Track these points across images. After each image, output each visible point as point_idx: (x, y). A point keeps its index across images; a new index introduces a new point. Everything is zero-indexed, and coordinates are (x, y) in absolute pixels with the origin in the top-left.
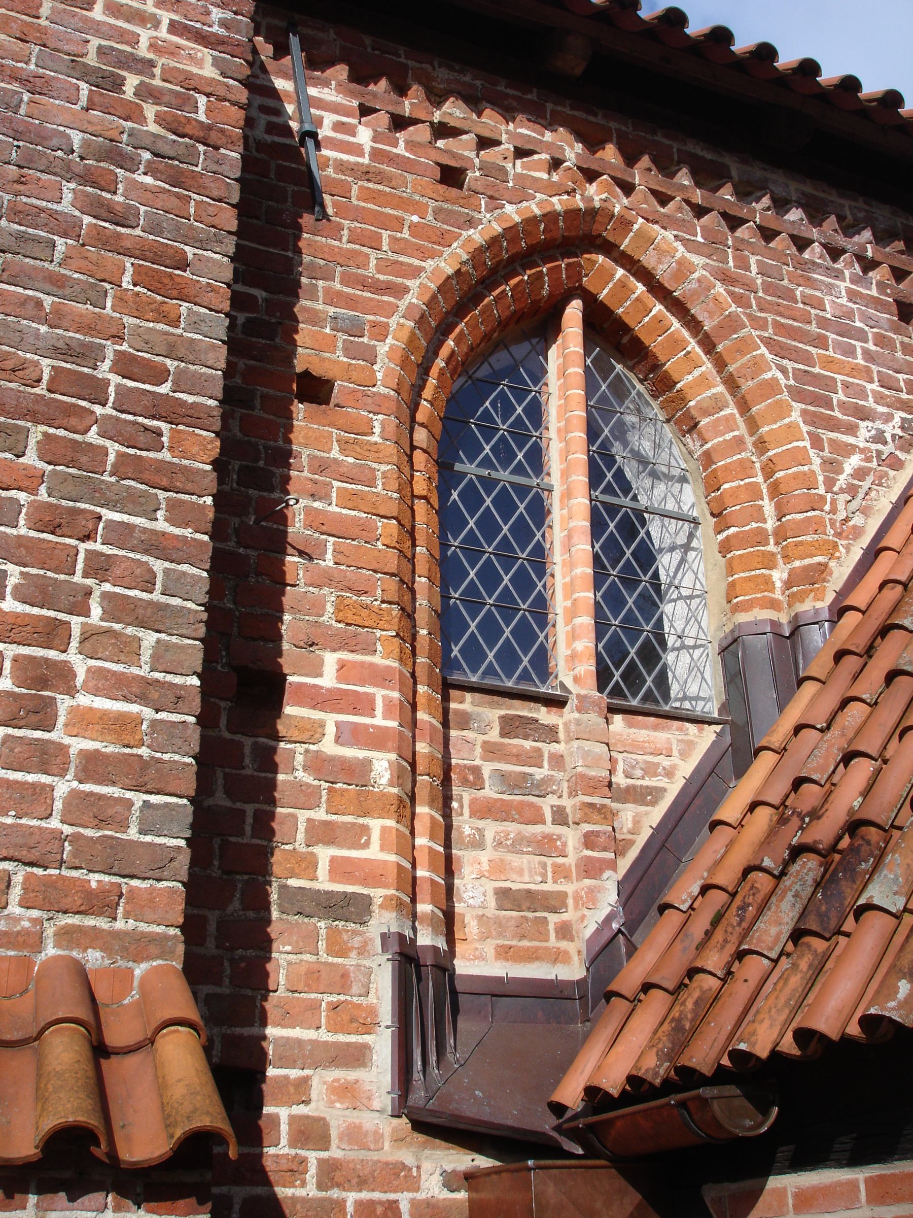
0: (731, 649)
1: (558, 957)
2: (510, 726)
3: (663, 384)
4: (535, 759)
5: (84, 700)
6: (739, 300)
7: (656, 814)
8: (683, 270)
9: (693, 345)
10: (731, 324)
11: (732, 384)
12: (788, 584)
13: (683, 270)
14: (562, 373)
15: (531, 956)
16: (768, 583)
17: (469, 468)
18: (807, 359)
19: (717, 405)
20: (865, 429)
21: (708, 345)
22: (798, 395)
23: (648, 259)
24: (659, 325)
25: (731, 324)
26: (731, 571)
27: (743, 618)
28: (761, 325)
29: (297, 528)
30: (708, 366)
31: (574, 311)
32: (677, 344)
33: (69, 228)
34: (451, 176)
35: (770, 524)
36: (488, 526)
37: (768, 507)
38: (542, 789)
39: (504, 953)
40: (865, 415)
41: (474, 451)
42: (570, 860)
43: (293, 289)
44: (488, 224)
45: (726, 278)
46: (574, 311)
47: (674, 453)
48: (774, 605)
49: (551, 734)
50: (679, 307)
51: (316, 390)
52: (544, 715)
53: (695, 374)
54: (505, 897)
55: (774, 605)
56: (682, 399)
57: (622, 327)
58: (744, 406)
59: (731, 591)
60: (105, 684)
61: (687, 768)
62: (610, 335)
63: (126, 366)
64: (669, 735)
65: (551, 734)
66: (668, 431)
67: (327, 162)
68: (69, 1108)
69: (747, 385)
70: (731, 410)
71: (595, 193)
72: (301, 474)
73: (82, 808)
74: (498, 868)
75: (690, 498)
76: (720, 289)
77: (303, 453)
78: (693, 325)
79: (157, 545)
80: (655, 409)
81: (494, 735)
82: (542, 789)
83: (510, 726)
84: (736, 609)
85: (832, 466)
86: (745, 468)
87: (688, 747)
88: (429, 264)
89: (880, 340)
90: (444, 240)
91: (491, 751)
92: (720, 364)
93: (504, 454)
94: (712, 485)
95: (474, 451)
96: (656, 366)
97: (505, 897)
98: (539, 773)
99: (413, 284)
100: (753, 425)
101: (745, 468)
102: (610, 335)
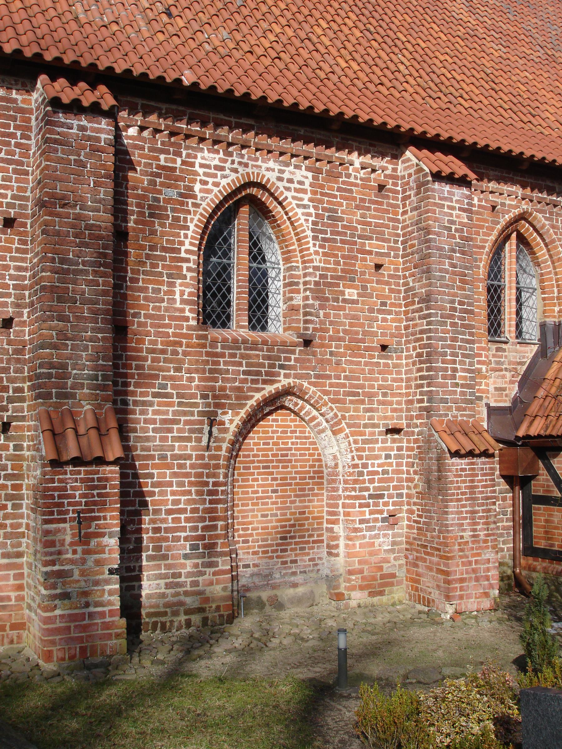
0: (543, 326)
1: (505, 401)
2: (498, 349)
3: (533, 253)
4: (501, 357)
5: (460, 374)
6: (556, 233)
7: (525, 368)
8: (544, 226)
9: (542, 245)
10: (553, 241)
11: (551, 256)
12: (559, 312)
13: (544, 226)
14: (510, 251)
15: (500, 401)
16: (554, 310)
19: (546, 261)
21: (546, 245)
23: (535, 223)
24: (535, 239)
25: (553, 241)
26: (545, 305)
27: (547, 320)
30: (545, 250)
32: (538, 244)
35: (556, 295)
37: (556, 290)
38: (503, 363)
39: (496, 401)
42: (508, 380)
45: (553, 227)
46: (514, 235)
47: (531, 269)
48: (555, 317)
49: (504, 350)
50: (541, 235)
52: (504, 346)
53: (542, 252)
54: (496, 389)
55: (555, 317)
56: (537, 258)
57: (525, 238)
58: (553, 263)
59: (544, 312)
60: (464, 370)
61: (531, 355)
62: (522, 240)
64: (528, 348)
65: (504, 350)
66: (531, 264)
69: (555, 258)
70: (549, 263)
73: (463, 393)
74: (495, 383)
75: (535, 283)
76: (551, 231)
78: (543, 240)
80: (529, 258)
81: (494, 352)
82: (503, 363)
83: (498, 349)
84: (545, 316)
86: (551, 279)
87: (532, 350)
88: (490, 238)
90: (493, 229)
91: (494, 356)
92: (549, 251)
94: (542, 281)
96: (532, 249)
97: (496, 389)
98: (502, 360)
99: (487, 245)
100: (555, 268)
101: (551, 279)
102: (522, 240)
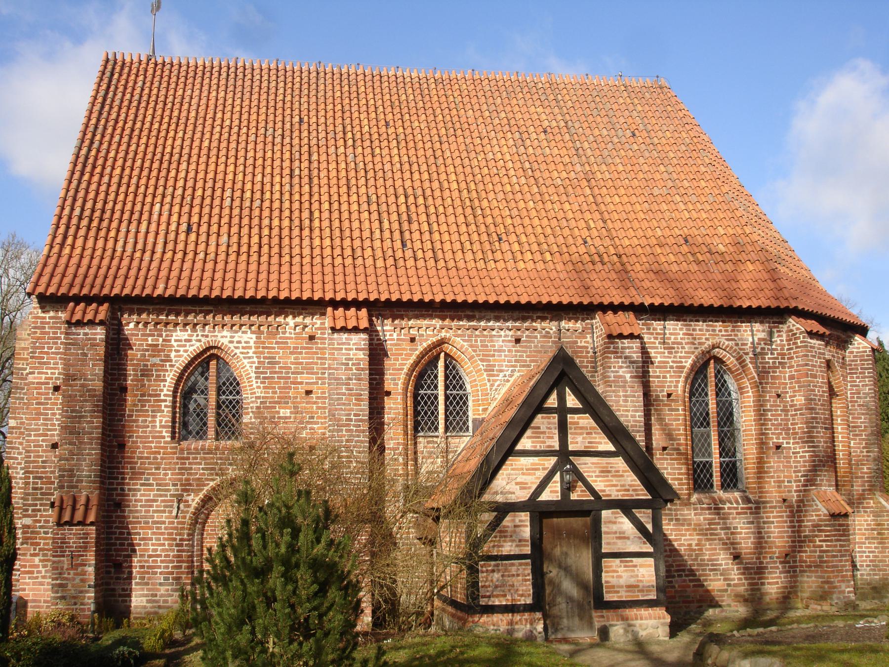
2: (428, 442)
6: (475, 351)
8: (462, 346)
13: (462, 346)
17: (422, 392)
18: (489, 361)
20: (502, 374)
22: (486, 370)
28: (478, 355)
29: (386, 420)
31: (442, 355)
33: (344, 394)
34: (413, 340)
36: (426, 403)
40: (501, 371)
41: (422, 387)
43: (383, 374)
44: (420, 349)
45: (471, 346)
51: (388, 394)
63: (355, 415)
67: (389, 345)
68: (355, 324)
71: (443, 334)
72: (386, 410)
77: (386, 406)
79: (362, 442)
85: (492, 385)
89: (509, 351)
90: (411, 355)
93: (429, 387)
95: (422, 387)
